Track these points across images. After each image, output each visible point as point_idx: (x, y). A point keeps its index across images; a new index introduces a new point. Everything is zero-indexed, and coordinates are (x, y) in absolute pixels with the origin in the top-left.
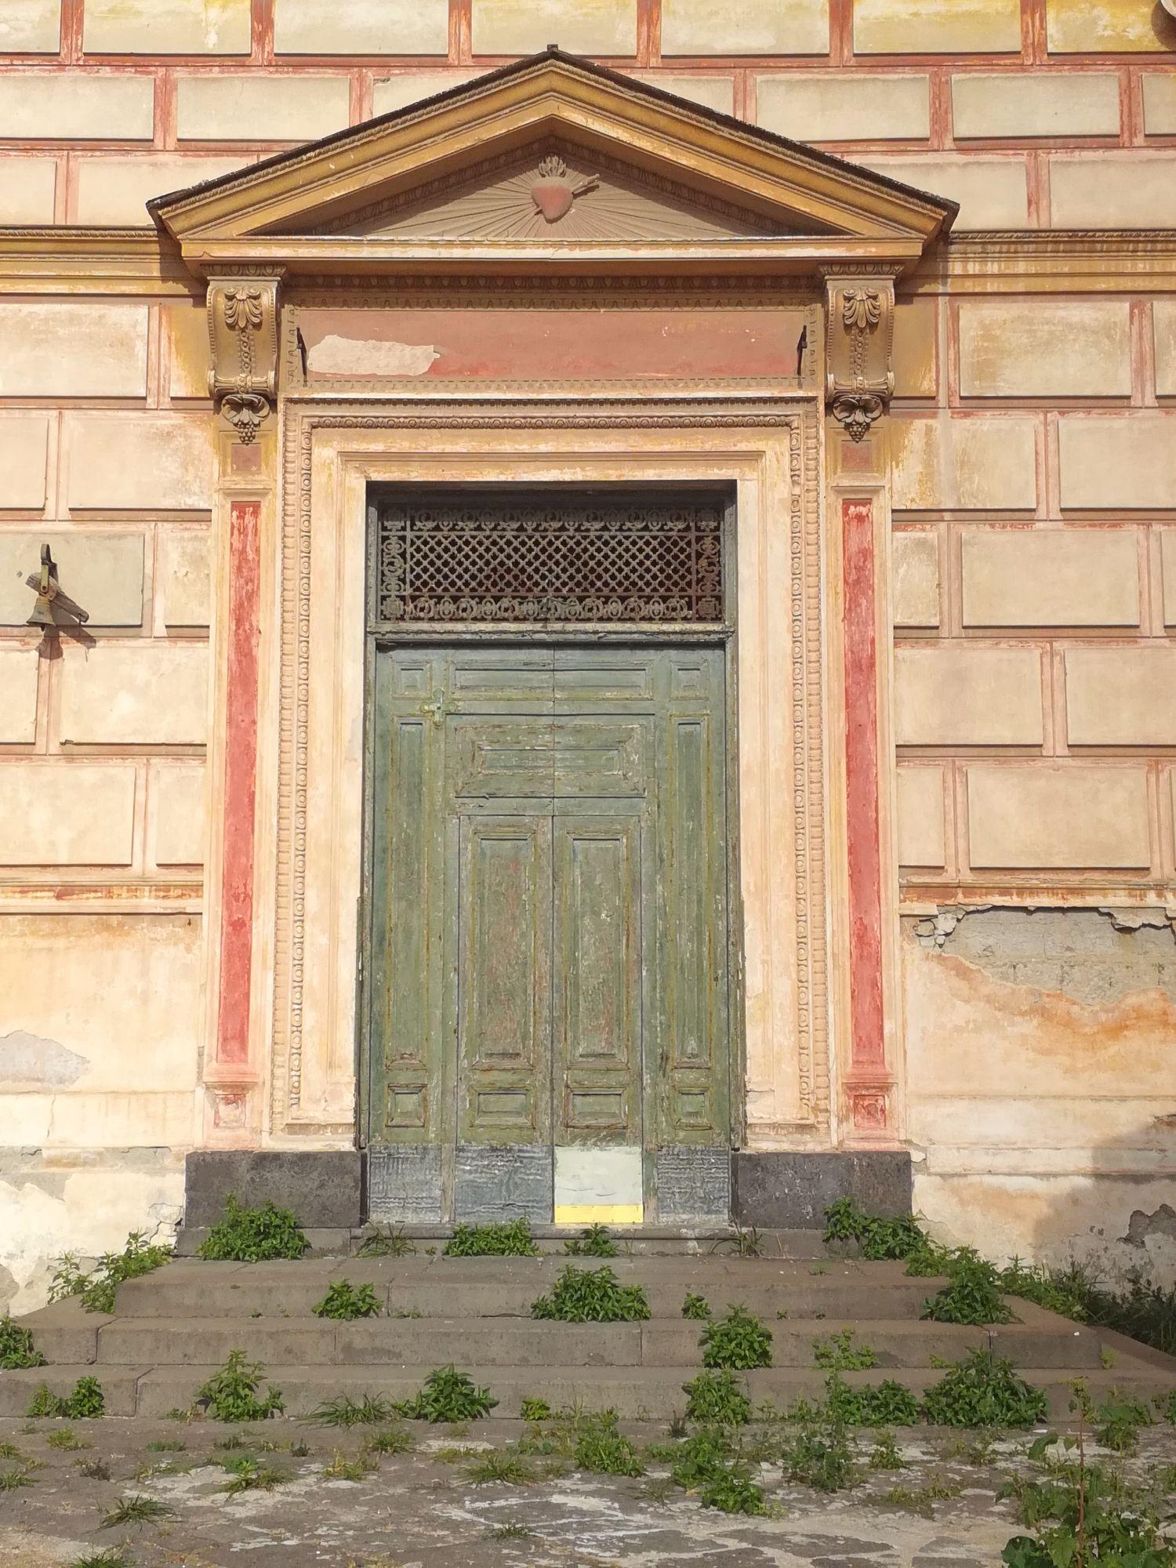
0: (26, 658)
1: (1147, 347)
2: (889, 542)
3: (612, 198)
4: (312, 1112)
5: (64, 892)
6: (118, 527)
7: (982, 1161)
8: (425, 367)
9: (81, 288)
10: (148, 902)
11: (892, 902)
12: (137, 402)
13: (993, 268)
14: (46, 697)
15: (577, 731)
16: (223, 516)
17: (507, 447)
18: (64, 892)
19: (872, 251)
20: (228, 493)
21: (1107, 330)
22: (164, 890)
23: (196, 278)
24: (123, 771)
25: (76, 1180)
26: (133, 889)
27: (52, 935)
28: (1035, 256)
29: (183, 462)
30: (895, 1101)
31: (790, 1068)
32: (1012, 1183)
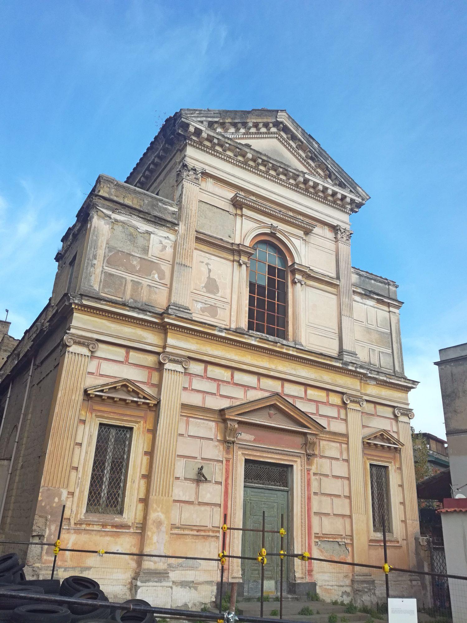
0: (194, 485)
1: (181, 309)
2: (313, 478)
3: (279, 416)
4: (235, 575)
5: (198, 531)
6: (208, 462)
7: (324, 583)
8: (253, 439)
9: (205, 418)
10: (211, 534)
11: (313, 540)
12: (212, 439)
13: (324, 436)
14: (197, 494)
15: (268, 505)
16: (224, 462)
17: (264, 455)
18: (198, 531)
19: (314, 432)
20: (226, 458)
21: (337, 448)
22: (213, 531)
23: (225, 421)
24: (208, 508)
25: (200, 587)
26: (209, 531)
27: (196, 539)
28: (329, 435)
29: (214, 451)
30: (314, 573)
31: (300, 568)
32: (328, 587)
